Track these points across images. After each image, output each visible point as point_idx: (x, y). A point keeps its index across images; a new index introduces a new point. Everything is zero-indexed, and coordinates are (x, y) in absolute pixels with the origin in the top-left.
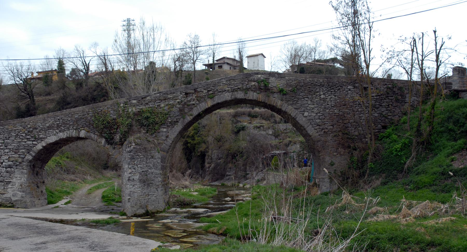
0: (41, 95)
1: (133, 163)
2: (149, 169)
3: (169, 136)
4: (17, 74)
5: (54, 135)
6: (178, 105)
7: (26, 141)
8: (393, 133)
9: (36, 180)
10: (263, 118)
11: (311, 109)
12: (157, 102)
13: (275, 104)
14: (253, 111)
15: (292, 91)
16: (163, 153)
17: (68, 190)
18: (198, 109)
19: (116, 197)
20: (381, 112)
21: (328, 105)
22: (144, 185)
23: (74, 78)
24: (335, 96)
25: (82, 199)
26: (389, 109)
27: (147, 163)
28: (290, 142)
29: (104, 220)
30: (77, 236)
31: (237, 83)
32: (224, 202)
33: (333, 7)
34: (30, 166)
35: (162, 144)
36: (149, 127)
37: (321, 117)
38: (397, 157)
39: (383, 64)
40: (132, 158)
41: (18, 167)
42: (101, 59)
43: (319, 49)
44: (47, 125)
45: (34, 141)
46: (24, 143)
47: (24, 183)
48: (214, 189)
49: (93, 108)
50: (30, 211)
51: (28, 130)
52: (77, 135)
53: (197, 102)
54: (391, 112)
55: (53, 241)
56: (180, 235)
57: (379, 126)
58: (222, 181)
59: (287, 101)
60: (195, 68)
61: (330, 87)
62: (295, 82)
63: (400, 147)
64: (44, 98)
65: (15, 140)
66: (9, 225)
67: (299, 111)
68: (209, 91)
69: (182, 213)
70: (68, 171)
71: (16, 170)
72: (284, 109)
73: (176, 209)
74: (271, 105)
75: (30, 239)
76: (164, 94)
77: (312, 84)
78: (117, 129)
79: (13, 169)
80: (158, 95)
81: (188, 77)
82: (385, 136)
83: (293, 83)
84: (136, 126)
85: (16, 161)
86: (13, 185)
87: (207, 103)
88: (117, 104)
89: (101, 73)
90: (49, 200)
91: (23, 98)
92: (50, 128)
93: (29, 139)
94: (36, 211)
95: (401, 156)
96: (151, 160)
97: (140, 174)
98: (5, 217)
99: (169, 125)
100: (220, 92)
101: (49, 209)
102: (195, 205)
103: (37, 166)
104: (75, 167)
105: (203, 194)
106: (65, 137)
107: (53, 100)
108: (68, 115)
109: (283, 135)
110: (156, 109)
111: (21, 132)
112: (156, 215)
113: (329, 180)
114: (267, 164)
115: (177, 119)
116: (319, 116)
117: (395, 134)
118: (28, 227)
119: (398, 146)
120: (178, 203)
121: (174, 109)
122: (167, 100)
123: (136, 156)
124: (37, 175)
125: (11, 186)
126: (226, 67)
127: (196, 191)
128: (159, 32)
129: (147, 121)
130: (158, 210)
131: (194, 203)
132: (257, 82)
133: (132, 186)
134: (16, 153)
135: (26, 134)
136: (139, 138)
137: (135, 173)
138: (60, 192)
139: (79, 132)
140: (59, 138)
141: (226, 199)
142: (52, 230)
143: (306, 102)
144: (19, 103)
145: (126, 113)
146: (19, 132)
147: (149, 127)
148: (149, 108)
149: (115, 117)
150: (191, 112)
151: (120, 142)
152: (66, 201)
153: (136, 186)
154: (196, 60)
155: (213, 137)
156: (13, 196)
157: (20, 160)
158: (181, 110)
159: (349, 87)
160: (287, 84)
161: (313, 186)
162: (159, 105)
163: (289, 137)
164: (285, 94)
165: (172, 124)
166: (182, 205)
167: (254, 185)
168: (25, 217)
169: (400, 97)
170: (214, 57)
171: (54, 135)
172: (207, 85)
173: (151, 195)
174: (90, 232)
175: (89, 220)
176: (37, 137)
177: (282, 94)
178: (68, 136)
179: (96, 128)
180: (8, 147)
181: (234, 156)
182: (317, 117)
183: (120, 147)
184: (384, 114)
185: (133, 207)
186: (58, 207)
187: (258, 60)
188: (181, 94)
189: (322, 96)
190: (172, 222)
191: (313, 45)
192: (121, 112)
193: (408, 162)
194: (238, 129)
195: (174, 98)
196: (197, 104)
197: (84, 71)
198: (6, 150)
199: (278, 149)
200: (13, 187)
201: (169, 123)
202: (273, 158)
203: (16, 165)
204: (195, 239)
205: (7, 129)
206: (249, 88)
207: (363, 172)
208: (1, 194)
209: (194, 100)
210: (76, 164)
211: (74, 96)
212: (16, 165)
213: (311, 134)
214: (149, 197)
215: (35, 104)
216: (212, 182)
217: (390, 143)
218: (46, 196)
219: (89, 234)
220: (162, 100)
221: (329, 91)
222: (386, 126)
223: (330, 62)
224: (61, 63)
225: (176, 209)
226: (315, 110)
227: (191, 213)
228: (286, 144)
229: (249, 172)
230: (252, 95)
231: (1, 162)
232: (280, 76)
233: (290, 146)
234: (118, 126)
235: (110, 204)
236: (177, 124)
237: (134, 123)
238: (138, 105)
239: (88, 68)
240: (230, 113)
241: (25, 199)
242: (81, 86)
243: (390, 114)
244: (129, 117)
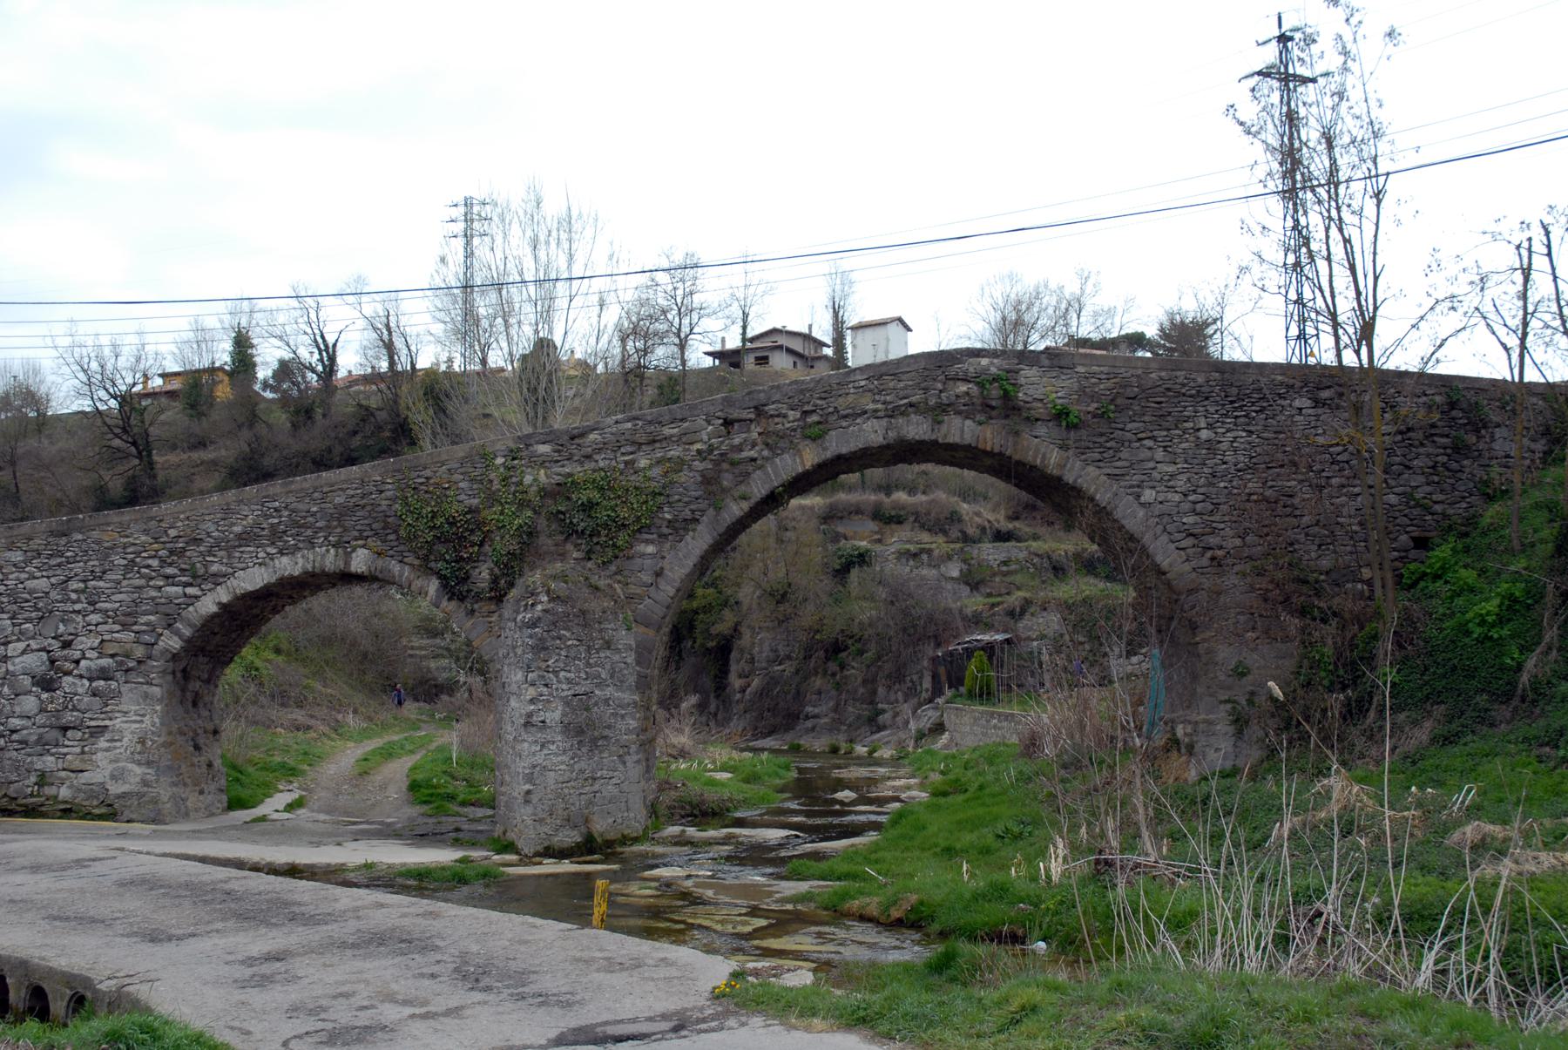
0: (174, 447)
1: (543, 665)
2: (598, 685)
3: (666, 572)
4: (99, 377)
5: (260, 564)
6: (696, 463)
7: (161, 583)
8: (1456, 563)
9: (191, 723)
10: (922, 526)
11: (1166, 478)
12: (623, 450)
13: (1038, 461)
14: (886, 500)
15: (1100, 415)
16: (642, 629)
17: (292, 763)
19: (456, 787)
20: (1408, 489)
21: (1225, 463)
22: (580, 742)
23: (285, 391)
24: (1251, 432)
25: (341, 793)
26: (1436, 479)
27: (588, 665)
28: (1027, 602)
29: (443, 868)
30: (393, 930)
31: (905, 388)
32: (837, 807)
33: (1242, 124)
34: (174, 673)
35: (641, 598)
36: (595, 540)
37: (1199, 507)
38: (1488, 644)
39: (1422, 318)
40: (540, 648)
41: (132, 676)
42: (375, 329)
43: (1093, 300)
44: (238, 529)
45: (191, 585)
46: (154, 593)
47: (153, 733)
48: (782, 760)
49: (398, 471)
50: (175, 832)
51: (168, 545)
52: (342, 567)
53: (766, 453)
54: (1442, 491)
55: (309, 951)
56: (745, 923)
57: (1404, 538)
58: (789, 737)
59: (1082, 451)
60: (684, 362)
61: (1232, 402)
62: (1110, 384)
63: (1497, 610)
64: (185, 456)
65: (125, 583)
66: (126, 884)
67: (1122, 484)
68: (806, 413)
69: (710, 843)
70: (282, 697)
71: (125, 688)
72: (1069, 478)
73: (684, 831)
74: (1024, 464)
75: (222, 942)
76: (650, 422)
78: (481, 545)
79: (114, 684)
80: (629, 425)
81: (666, 390)
82: (1425, 574)
83: (1102, 387)
84: (550, 536)
85: (127, 656)
86: (113, 740)
87: (801, 457)
88: (484, 456)
89: (373, 378)
90: (233, 793)
91: (117, 456)
92: (245, 538)
93: (174, 577)
94: (194, 831)
95: (1499, 642)
96: (602, 655)
97: (567, 703)
98: (100, 854)
99: (665, 531)
101: (234, 827)
102: (738, 815)
103: (195, 673)
104: (306, 681)
105: (752, 778)
106: (297, 573)
107: (214, 463)
108: (310, 495)
109: (997, 579)
110: (621, 474)
111: (144, 554)
112: (619, 849)
113: (1231, 729)
114: (950, 675)
115: (693, 511)
116: (1194, 503)
117: (1466, 566)
118: (194, 890)
119: (1492, 606)
120: (683, 808)
121: (684, 477)
122: (658, 445)
123: (553, 638)
124: (195, 704)
125: (107, 745)
126: (780, 362)
127: (724, 769)
128: (589, 233)
129: (589, 516)
130: (626, 833)
131: (736, 808)
132: (977, 384)
133: (538, 748)
134: (125, 626)
135: (163, 561)
136: (563, 577)
137: (549, 701)
138: (262, 769)
139: (348, 556)
140: (278, 575)
141: (840, 795)
142: (286, 904)
143: (1146, 454)
144: (102, 473)
145: (513, 489)
146: (138, 554)
147: (595, 540)
148: (594, 471)
149: (475, 501)
150: (742, 488)
151: (491, 590)
152: (288, 798)
154: (687, 336)
155: (759, 586)
156: (113, 777)
157: (139, 652)
158: (707, 481)
159: (1297, 403)
160: (1082, 391)
161: (1168, 751)
162: (632, 462)
163: (1019, 588)
164: (1075, 427)
165: (676, 529)
166: (696, 816)
167: (910, 749)
168: (164, 855)
169: (1474, 439)
170: (744, 328)
171: (260, 564)
172: (802, 392)
173: (602, 778)
174: (433, 915)
175: (390, 866)
176: (201, 572)
177: (1064, 424)
178: (310, 568)
179: (409, 540)
180: (97, 606)
181: (835, 649)
182: (1186, 506)
183: (493, 607)
184: (1417, 496)
185: (541, 821)
186: (263, 819)
187: (888, 340)
188: (709, 423)
189: (1204, 434)
190: (689, 877)
191: (1072, 289)
192: (496, 486)
193: (1530, 664)
194: (843, 560)
195: (685, 439)
196: (766, 459)
197: (320, 368)
198: (92, 616)
199: (989, 627)
200: (115, 748)
201: (665, 523)
202: (969, 658)
203: (127, 671)
204: (809, 939)
205: (98, 542)
206: (948, 405)
207: (1360, 701)
208: (73, 771)
209: (754, 445)
210: (306, 671)
211: (287, 451)
212: (127, 671)
213: (1165, 565)
214: (596, 787)
215: (155, 477)
216: (755, 737)
217: (1452, 598)
218: (223, 782)
219: (434, 923)
220: (641, 444)
221: (1226, 416)
222: (1426, 539)
223: (1123, 346)
224: (242, 343)
225: (684, 831)
227: (742, 843)
228: (1014, 610)
229: (885, 706)
230: (960, 430)
231: (75, 657)
232: (1055, 362)
233: (1027, 616)
234: (487, 536)
235: (440, 811)
236: (694, 530)
237: (542, 523)
238: (558, 461)
239: (332, 359)
240: (812, 508)
241: (153, 792)
242: (310, 418)
243: (1441, 497)
244: (523, 504)
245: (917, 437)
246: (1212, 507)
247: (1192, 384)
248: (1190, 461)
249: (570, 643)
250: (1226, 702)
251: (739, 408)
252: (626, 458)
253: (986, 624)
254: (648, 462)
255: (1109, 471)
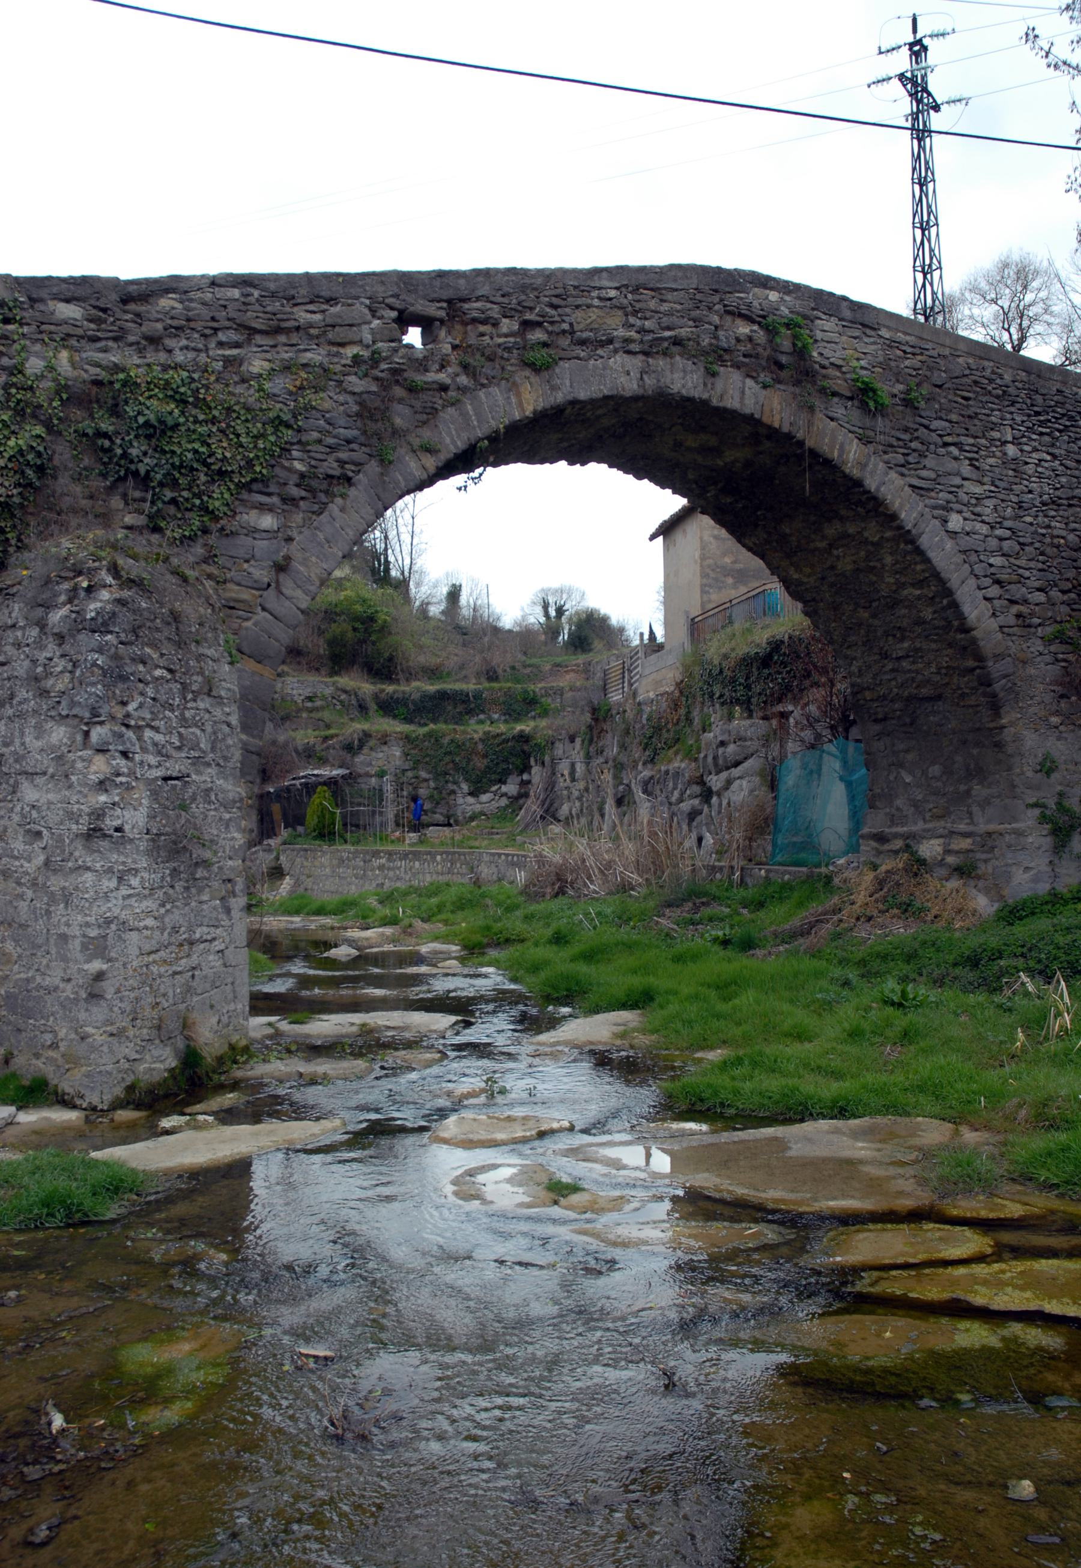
3: (295, 564)
12: (222, 336)
13: (836, 454)
16: (251, 665)
18: (464, 415)
21: (1030, 492)
24: (1054, 457)
27: (183, 721)
31: (669, 314)
53: (463, 380)
61: (1037, 414)
68: (527, 325)
76: (273, 295)
77: (976, 382)
80: (236, 293)
83: (907, 363)
84: (78, 479)
87: (518, 395)
100: (583, 343)
116: (1001, 539)
121: (324, 400)
122: (282, 338)
133: (113, 884)
143: (952, 465)
148: (165, 368)
150: (426, 434)
153: (135, 882)
172: (524, 289)
199: (323, 761)
201: (294, 479)
226: (987, 509)
233: (365, 750)
236: (343, 496)
238: (95, 339)
245: (684, 392)
246: (1018, 547)
247: (998, 381)
248: (997, 483)
249: (158, 673)
250: (1036, 805)
251: (424, 297)
252: (228, 352)
253: (320, 759)
254: (266, 365)
255: (916, 482)
